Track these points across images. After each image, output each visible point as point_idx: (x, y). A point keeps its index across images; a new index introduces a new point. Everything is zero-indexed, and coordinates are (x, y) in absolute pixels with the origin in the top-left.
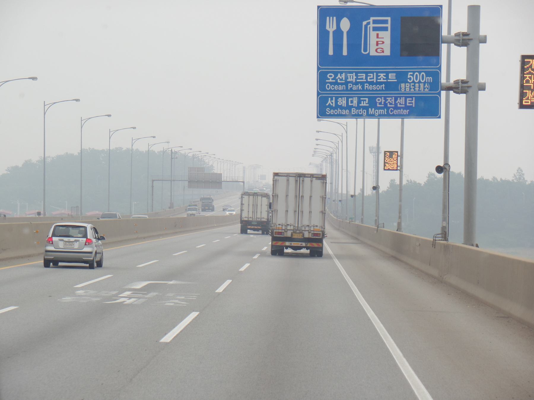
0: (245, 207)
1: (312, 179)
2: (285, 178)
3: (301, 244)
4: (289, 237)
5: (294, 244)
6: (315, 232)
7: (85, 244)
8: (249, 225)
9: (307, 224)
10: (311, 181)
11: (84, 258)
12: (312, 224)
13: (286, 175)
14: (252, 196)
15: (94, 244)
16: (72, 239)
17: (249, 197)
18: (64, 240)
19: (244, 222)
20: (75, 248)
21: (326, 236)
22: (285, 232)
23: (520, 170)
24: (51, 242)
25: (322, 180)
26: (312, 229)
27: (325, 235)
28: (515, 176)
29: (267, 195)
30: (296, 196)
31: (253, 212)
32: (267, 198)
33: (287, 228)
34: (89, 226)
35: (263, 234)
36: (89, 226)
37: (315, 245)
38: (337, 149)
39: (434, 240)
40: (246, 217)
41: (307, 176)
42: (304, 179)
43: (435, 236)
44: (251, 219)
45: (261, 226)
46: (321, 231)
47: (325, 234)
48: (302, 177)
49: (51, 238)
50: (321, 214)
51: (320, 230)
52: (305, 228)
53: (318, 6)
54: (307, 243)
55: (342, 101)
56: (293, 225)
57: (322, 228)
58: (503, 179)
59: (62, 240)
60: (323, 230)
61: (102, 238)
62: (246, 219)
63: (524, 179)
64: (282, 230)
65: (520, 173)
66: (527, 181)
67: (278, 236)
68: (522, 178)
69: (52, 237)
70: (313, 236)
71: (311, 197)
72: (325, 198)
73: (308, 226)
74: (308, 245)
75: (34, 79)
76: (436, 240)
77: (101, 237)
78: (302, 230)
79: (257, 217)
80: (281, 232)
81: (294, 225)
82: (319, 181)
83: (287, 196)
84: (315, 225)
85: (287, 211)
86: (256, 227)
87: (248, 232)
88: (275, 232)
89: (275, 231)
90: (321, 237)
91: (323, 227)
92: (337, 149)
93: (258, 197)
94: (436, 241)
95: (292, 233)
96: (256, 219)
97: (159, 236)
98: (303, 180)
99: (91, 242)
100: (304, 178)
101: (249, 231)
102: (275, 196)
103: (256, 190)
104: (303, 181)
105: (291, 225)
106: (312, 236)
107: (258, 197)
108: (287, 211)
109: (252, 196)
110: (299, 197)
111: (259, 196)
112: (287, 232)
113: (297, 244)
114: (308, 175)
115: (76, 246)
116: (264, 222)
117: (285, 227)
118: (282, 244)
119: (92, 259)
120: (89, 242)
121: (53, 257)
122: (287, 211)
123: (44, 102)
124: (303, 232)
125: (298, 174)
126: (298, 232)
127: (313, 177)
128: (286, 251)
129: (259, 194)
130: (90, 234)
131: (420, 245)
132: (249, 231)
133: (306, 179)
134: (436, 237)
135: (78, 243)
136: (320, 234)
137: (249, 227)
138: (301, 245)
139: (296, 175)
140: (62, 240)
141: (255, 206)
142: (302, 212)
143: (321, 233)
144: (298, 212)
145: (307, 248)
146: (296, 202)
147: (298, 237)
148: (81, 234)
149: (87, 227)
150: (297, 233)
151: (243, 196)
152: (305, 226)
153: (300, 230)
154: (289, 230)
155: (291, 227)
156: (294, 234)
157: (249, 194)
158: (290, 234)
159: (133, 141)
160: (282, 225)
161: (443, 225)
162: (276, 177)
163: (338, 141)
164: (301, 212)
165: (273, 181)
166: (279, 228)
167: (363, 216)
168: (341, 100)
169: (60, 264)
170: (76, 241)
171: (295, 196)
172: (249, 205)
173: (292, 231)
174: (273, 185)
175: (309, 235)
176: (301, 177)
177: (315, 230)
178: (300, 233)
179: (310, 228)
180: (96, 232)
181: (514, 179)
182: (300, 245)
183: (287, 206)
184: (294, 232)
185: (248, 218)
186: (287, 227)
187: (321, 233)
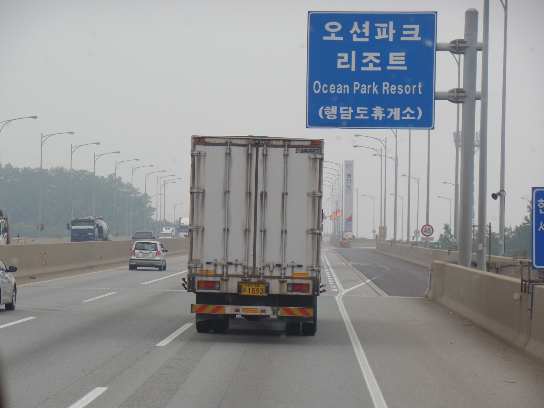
1: (286, 152)
2: (222, 149)
3: (263, 311)
4: (232, 294)
6: (297, 281)
7: (156, 255)
10: (286, 156)
11: (156, 264)
12: (289, 262)
13: (223, 141)
16: (148, 252)
20: (150, 257)
21: (324, 291)
25: (311, 152)
26: (289, 273)
27: (321, 287)
30: (248, 194)
33: (227, 272)
34: (158, 243)
36: (158, 243)
37: (296, 312)
38: (337, 180)
41: (274, 143)
42: (267, 150)
47: (321, 284)
48: (262, 146)
49: (134, 251)
50: (310, 236)
51: (307, 276)
52: (271, 271)
53: (306, 128)
54: (276, 308)
55: (331, 111)
56: (241, 264)
57: (313, 270)
59: (141, 252)
60: (315, 275)
61: (166, 251)
67: (205, 291)
69: (134, 250)
70: (292, 292)
71: (284, 195)
73: (279, 266)
78: (264, 277)
80: (214, 283)
81: (245, 263)
82: (305, 156)
83: (226, 193)
84: (297, 263)
85: (226, 230)
88: (199, 282)
89: (198, 279)
90: (310, 293)
91: (316, 267)
92: (337, 180)
95: (239, 283)
97: (71, 271)
98: (265, 153)
100: (268, 149)
102: (198, 193)
104: (265, 156)
105: (236, 265)
106: (288, 291)
108: (226, 230)
112: (227, 280)
114: (276, 140)
115: (150, 256)
117: (223, 269)
118: (215, 310)
119: (161, 264)
120: (158, 253)
122: (228, 230)
124: (268, 280)
125: (254, 140)
126: (254, 280)
130: (159, 248)
131: (432, 269)
133: (271, 150)
135: (151, 254)
136: (308, 285)
138: (263, 314)
139: (248, 141)
140: (141, 252)
142: (265, 232)
143: (310, 282)
147: (255, 294)
148: (153, 248)
150: (253, 283)
152: (271, 266)
153: (259, 277)
155: (236, 269)
156: (244, 286)
158: (235, 285)
160: (216, 265)
162: (199, 148)
164: (261, 231)
165: (192, 155)
166: (207, 271)
168: (330, 109)
169: (138, 268)
170: (150, 253)
171: (247, 193)
173: (240, 280)
174: (193, 166)
175: (281, 288)
176: (261, 146)
177: (295, 276)
179: (283, 271)
180: (162, 247)
182: (258, 314)
183: (227, 218)
184: (245, 282)
186: (227, 268)
187: (310, 282)
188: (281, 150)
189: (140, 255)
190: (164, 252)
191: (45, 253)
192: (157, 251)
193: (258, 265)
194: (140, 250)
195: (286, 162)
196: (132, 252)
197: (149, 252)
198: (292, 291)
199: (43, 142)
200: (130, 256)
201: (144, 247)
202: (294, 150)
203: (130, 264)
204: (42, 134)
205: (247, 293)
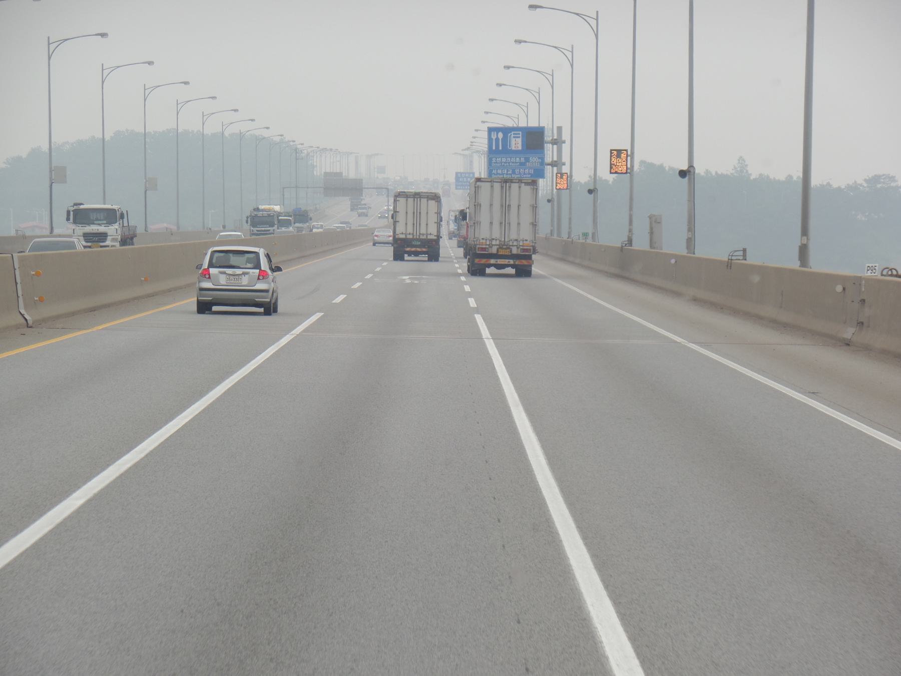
0: (401, 217)
3: (509, 262)
5: (500, 261)
7: (259, 279)
8: (408, 246)
9: (515, 238)
10: (520, 187)
12: (521, 238)
14: (412, 197)
15: (271, 277)
17: (407, 200)
18: (227, 272)
19: (399, 242)
20: (243, 284)
22: (490, 247)
23: (741, 159)
24: (207, 276)
28: (735, 167)
29: (435, 196)
30: (502, 206)
31: (414, 224)
32: (436, 202)
34: (262, 252)
35: (430, 260)
36: (262, 252)
37: (525, 262)
39: (729, 259)
40: (402, 233)
43: (731, 255)
44: (411, 237)
45: (426, 247)
46: (532, 246)
48: (509, 182)
50: (531, 226)
52: (513, 243)
56: (499, 239)
57: (533, 242)
58: (719, 173)
59: (224, 273)
60: (533, 244)
62: (403, 236)
63: (747, 171)
64: (486, 245)
65: (742, 164)
66: (751, 174)
68: (745, 171)
69: (208, 268)
71: (519, 206)
72: (536, 207)
73: (516, 240)
74: (517, 263)
75: (103, 36)
76: (732, 260)
77: (275, 267)
79: (421, 233)
80: (485, 248)
83: (491, 205)
84: (525, 238)
85: (491, 223)
86: (419, 249)
87: (406, 259)
89: (478, 246)
93: (422, 199)
94: (733, 261)
96: (419, 236)
99: (267, 275)
101: (406, 257)
102: (478, 205)
103: (413, 189)
104: (510, 187)
107: (422, 199)
108: (491, 223)
109: (412, 199)
110: (506, 208)
111: (422, 198)
112: (492, 247)
113: (503, 262)
115: (245, 280)
116: (432, 240)
120: (263, 275)
121: (211, 299)
123: (103, 64)
124: (511, 247)
126: (504, 247)
127: (521, 182)
128: (488, 271)
129: (424, 196)
132: (406, 257)
134: (732, 256)
136: (530, 249)
137: (408, 249)
140: (224, 273)
141: (417, 214)
143: (531, 248)
144: (505, 224)
145: (513, 266)
146: (502, 212)
149: (259, 253)
151: (398, 199)
153: (507, 245)
154: (494, 245)
156: (499, 250)
157: (407, 195)
159: (179, 106)
160: (486, 240)
161: (803, 242)
162: (478, 183)
163: (518, 115)
165: (475, 187)
167: (805, 238)
169: (215, 308)
170: (244, 274)
172: (407, 213)
173: (498, 247)
174: (475, 192)
175: (517, 251)
178: (509, 248)
181: (734, 172)
183: (492, 217)
184: (500, 248)
185: (406, 234)
187: (531, 248)
188: (517, 185)
189: (220, 278)
190: (274, 272)
191: (38, 274)
192: (260, 269)
193: (506, 240)
194: (220, 267)
195: (520, 190)
196: (202, 273)
197: (241, 273)
198: (523, 252)
199: (104, 78)
200: (199, 282)
201: (229, 261)
202: (523, 184)
203: (198, 300)
204: (49, 38)
205: (501, 253)
